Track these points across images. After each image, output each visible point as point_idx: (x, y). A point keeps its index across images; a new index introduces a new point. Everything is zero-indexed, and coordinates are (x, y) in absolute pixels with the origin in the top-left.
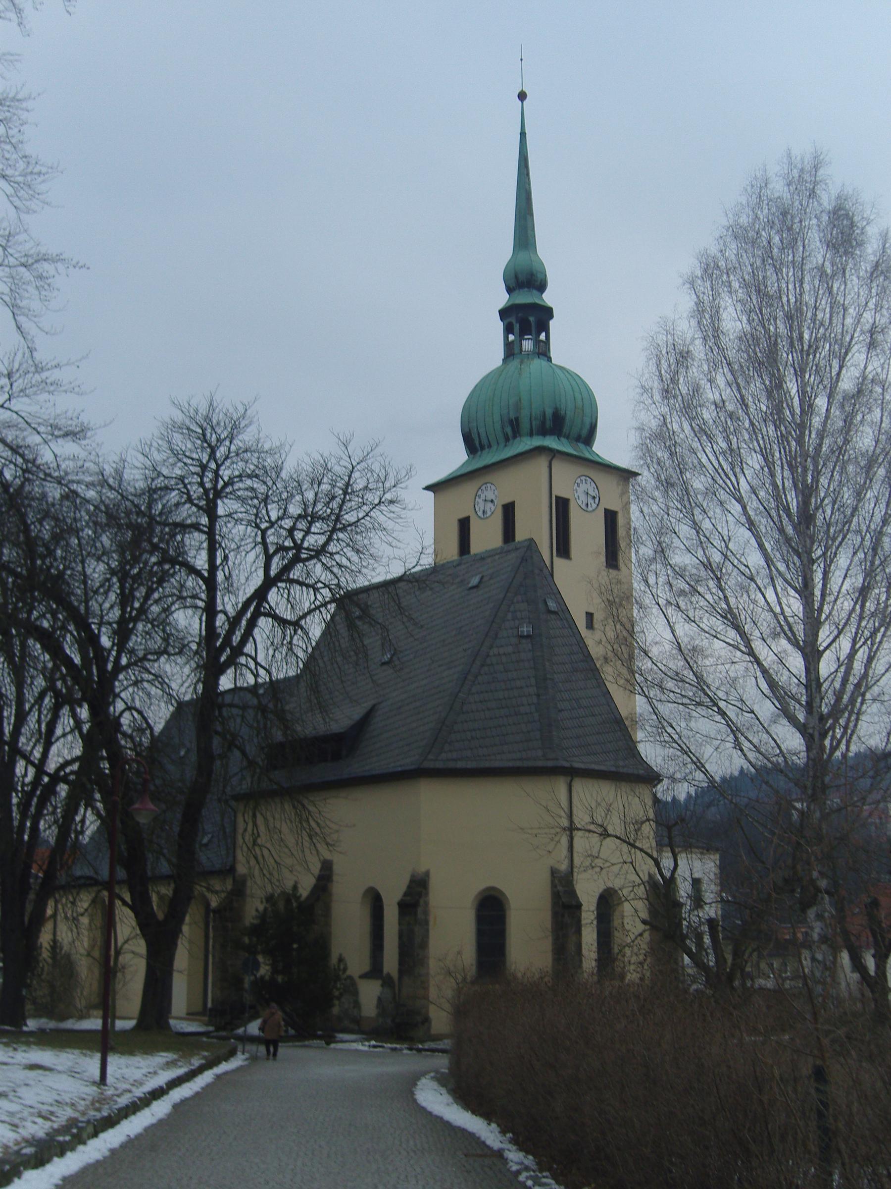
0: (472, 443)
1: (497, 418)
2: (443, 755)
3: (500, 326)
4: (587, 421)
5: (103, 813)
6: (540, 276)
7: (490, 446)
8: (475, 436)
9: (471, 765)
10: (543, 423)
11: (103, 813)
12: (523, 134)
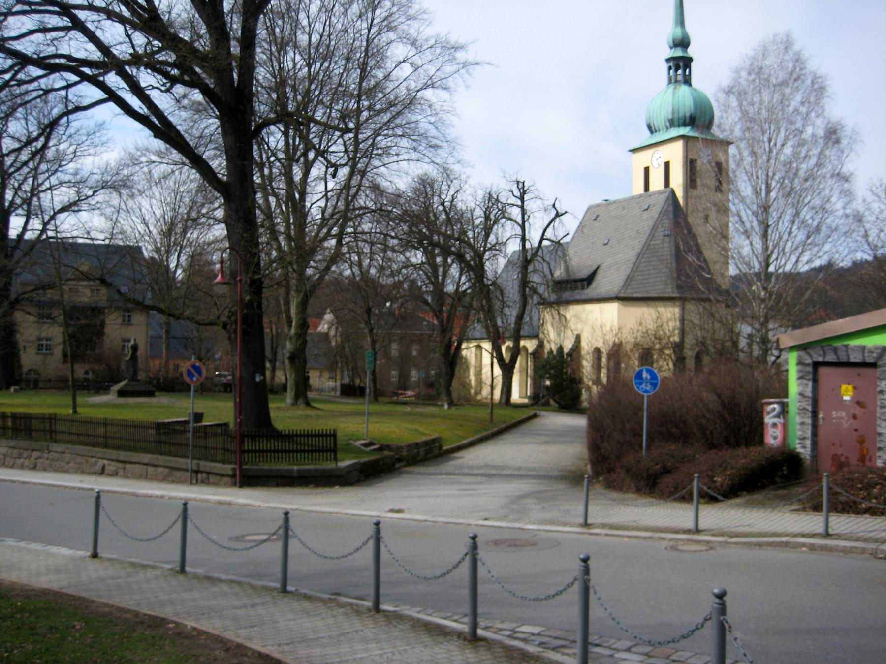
1: (662, 118)
2: (628, 291)
3: (665, 66)
4: (708, 117)
5: (48, 61)
6: (686, 41)
7: (659, 131)
8: (652, 125)
9: (639, 295)
10: (685, 121)
11: (48, 61)
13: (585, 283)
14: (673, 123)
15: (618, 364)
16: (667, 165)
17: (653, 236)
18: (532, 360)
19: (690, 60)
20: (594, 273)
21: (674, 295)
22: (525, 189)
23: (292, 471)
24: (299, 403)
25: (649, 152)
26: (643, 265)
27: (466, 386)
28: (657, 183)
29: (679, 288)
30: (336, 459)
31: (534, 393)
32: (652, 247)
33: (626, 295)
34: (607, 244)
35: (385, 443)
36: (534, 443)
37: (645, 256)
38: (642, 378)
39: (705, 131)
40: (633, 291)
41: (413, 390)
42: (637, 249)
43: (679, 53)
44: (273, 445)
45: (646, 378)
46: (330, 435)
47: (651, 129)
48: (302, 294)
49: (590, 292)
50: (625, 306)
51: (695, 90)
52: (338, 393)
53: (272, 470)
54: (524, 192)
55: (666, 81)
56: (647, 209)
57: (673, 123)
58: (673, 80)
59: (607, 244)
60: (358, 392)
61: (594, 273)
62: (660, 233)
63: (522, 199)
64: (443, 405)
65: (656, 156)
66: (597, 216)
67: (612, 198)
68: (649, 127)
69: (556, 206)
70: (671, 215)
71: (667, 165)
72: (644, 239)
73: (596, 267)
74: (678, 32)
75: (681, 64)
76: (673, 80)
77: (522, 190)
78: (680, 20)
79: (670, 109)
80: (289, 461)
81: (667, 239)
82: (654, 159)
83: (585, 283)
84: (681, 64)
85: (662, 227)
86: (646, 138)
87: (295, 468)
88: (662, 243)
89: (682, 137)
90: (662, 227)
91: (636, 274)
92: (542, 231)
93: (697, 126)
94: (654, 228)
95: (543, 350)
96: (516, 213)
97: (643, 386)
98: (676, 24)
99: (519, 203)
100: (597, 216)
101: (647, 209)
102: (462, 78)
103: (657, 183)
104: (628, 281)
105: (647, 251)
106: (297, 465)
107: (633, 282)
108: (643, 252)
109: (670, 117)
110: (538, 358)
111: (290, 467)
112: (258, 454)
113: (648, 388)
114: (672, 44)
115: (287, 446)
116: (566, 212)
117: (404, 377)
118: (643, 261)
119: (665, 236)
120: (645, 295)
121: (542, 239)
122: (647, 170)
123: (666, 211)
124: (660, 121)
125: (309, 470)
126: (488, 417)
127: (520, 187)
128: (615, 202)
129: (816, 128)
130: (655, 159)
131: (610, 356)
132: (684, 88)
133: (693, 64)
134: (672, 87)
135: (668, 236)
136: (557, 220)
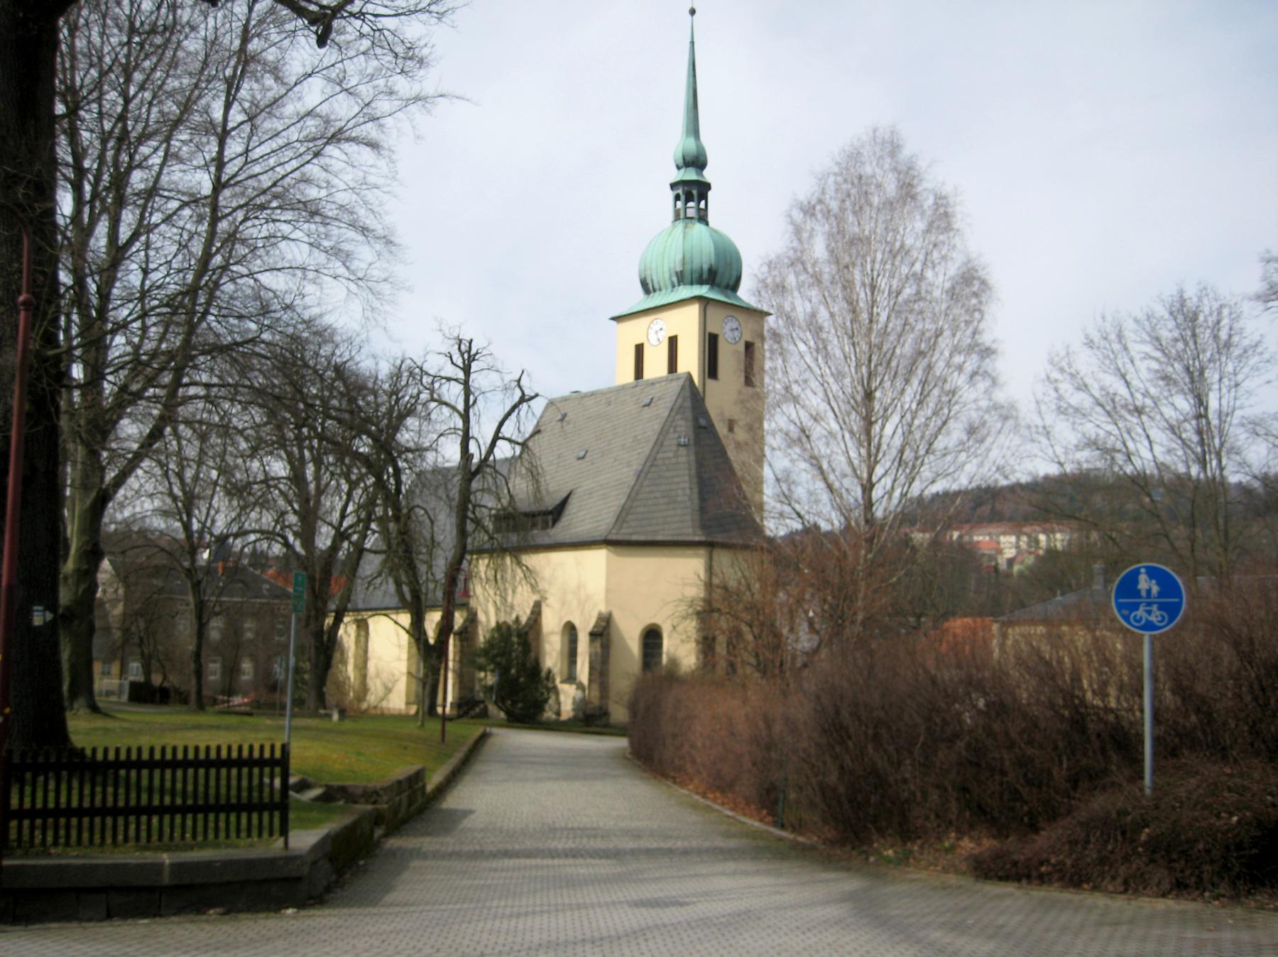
0: (647, 287)
1: (666, 269)
2: (623, 531)
3: (670, 195)
4: (735, 274)
6: (701, 159)
8: (649, 281)
9: (642, 538)
10: (701, 275)
12: (692, 43)
13: (550, 518)
14: (681, 278)
15: (606, 647)
16: (673, 342)
17: (662, 445)
18: (458, 643)
19: (707, 186)
20: (564, 503)
21: (697, 539)
22: (473, 352)
23: (157, 868)
24: (76, 706)
25: (644, 321)
26: (647, 489)
27: (341, 686)
28: (656, 366)
29: (704, 527)
30: (284, 832)
31: (460, 698)
32: (660, 462)
33: (620, 537)
34: (583, 458)
35: (336, 783)
36: (549, 779)
37: (650, 476)
38: (1137, 593)
39: (729, 292)
40: (630, 531)
41: (245, 694)
42: (636, 466)
43: (691, 175)
44: (73, 794)
45: (1149, 591)
46: (272, 762)
47: (647, 288)
48: (93, 495)
49: (560, 532)
50: (618, 554)
51: (715, 231)
52: (125, 697)
53: (95, 867)
54: (472, 359)
55: (671, 216)
56: (648, 405)
57: (681, 278)
58: (682, 216)
59: (583, 458)
60: (158, 696)
61: (564, 503)
62: (671, 440)
63: (467, 370)
64: (329, 716)
65: (656, 327)
66: (564, 416)
67: (584, 389)
68: (644, 284)
69: (522, 383)
70: (689, 414)
71: (673, 342)
72: (647, 450)
73: (564, 495)
74: (691, 144)
75: (695, 192)
76: (682, 216)
77: (466, 356)
78: (693, 128)
79: (680, 256)
80: (138, 838)
81: (683, 451)
82: (652, 332)
83: (550, 518)
84: (695, 192)
85: (675, 431)
86: (638, 300)
87: (166, 858)
88: (676, 456)
89: (699, 299)
90: (675, 431)
91: (635, 504)
92: (497, 424)
93: (719, 286)
94: (663, 432)
95: (476, 628)
96: (453, 393)
97: (1141, 612)
98: (688, 134)
99: (461, 375)
100: (564, 416)
101: (648, 405)
102: (411, 121)
103: (656, 366)
104: (623, 516)
105: (650, 469)
106: (167, 849)
107: (630, 517)
108: (646, 470)
109: (679, 269)
110: (467, 640)
111: (149, 857)
112: (39, 822)
113: (1154, 618)
114: (681, 162)
115: (110, 795)
116: (537, 395)
117: (232, 670)
118: (646, 483)
119: (679, 445)
120: (650, 538)
121: (496, 437)
122: (639, 349)
123: (681, 407)
124: (662, 271)
125: (208, 864)
126: (438, 735)
127: (463, 348)
128: (593, 394)
129: (939, 279)
130: (654, 332)
131: (593, 635)
132: (698, 227)
133: (710, 194)
134: (680, 225)
135: (684, 445)
136: (524, 406)
